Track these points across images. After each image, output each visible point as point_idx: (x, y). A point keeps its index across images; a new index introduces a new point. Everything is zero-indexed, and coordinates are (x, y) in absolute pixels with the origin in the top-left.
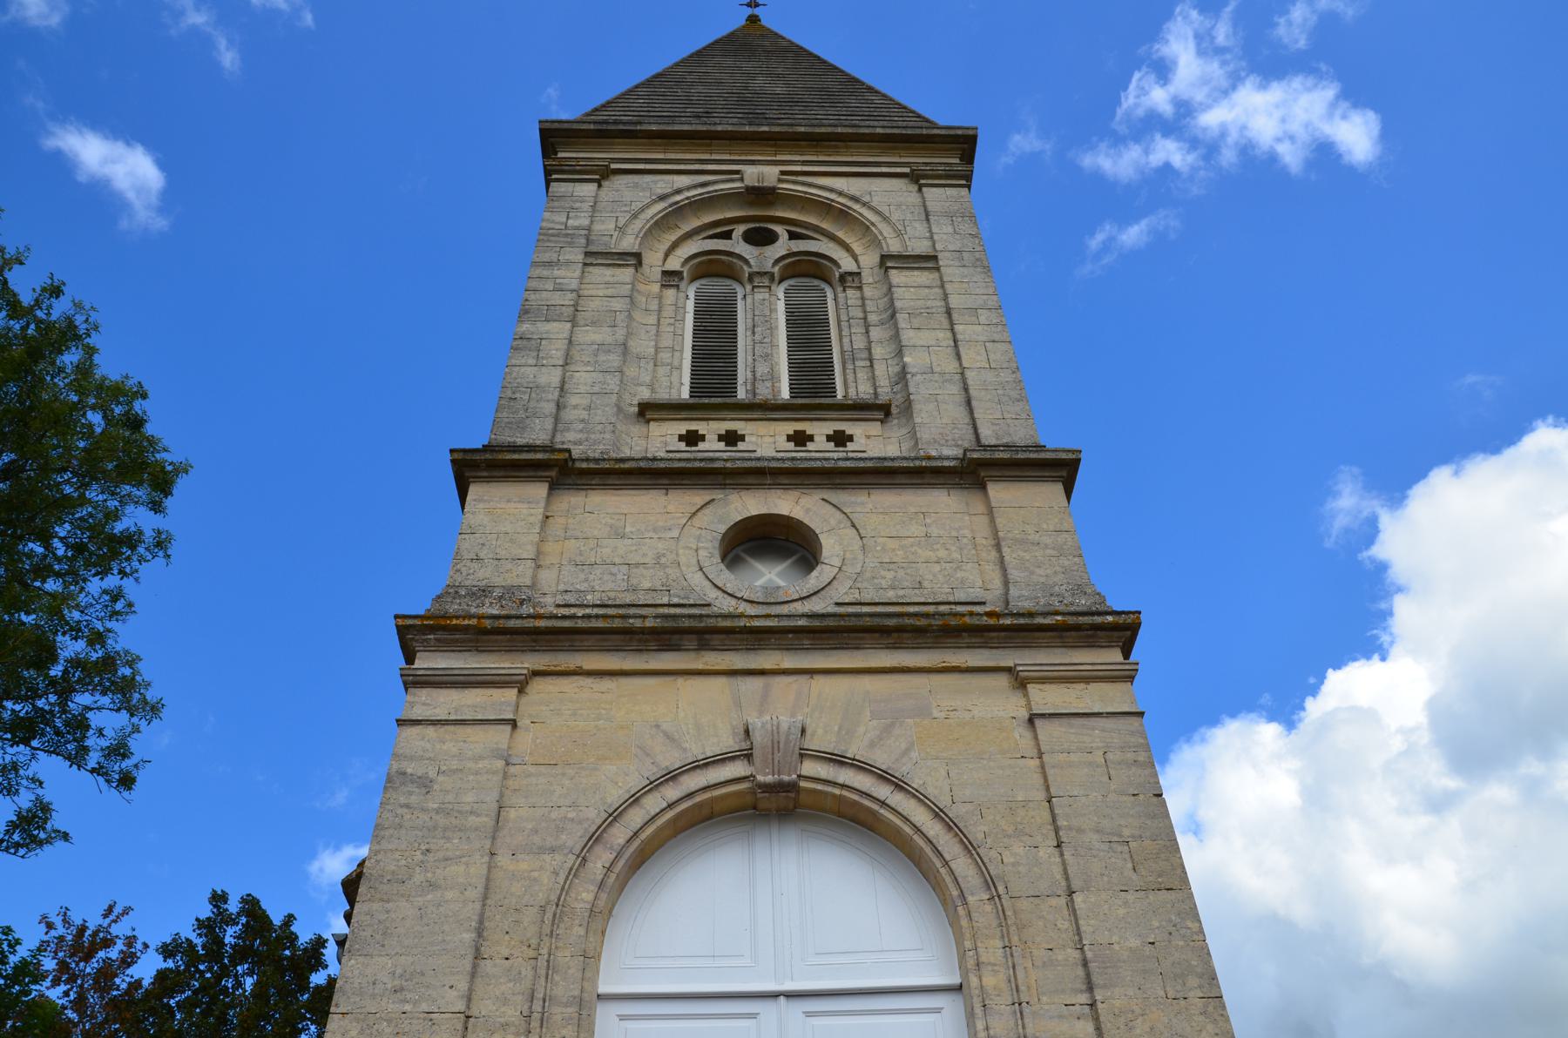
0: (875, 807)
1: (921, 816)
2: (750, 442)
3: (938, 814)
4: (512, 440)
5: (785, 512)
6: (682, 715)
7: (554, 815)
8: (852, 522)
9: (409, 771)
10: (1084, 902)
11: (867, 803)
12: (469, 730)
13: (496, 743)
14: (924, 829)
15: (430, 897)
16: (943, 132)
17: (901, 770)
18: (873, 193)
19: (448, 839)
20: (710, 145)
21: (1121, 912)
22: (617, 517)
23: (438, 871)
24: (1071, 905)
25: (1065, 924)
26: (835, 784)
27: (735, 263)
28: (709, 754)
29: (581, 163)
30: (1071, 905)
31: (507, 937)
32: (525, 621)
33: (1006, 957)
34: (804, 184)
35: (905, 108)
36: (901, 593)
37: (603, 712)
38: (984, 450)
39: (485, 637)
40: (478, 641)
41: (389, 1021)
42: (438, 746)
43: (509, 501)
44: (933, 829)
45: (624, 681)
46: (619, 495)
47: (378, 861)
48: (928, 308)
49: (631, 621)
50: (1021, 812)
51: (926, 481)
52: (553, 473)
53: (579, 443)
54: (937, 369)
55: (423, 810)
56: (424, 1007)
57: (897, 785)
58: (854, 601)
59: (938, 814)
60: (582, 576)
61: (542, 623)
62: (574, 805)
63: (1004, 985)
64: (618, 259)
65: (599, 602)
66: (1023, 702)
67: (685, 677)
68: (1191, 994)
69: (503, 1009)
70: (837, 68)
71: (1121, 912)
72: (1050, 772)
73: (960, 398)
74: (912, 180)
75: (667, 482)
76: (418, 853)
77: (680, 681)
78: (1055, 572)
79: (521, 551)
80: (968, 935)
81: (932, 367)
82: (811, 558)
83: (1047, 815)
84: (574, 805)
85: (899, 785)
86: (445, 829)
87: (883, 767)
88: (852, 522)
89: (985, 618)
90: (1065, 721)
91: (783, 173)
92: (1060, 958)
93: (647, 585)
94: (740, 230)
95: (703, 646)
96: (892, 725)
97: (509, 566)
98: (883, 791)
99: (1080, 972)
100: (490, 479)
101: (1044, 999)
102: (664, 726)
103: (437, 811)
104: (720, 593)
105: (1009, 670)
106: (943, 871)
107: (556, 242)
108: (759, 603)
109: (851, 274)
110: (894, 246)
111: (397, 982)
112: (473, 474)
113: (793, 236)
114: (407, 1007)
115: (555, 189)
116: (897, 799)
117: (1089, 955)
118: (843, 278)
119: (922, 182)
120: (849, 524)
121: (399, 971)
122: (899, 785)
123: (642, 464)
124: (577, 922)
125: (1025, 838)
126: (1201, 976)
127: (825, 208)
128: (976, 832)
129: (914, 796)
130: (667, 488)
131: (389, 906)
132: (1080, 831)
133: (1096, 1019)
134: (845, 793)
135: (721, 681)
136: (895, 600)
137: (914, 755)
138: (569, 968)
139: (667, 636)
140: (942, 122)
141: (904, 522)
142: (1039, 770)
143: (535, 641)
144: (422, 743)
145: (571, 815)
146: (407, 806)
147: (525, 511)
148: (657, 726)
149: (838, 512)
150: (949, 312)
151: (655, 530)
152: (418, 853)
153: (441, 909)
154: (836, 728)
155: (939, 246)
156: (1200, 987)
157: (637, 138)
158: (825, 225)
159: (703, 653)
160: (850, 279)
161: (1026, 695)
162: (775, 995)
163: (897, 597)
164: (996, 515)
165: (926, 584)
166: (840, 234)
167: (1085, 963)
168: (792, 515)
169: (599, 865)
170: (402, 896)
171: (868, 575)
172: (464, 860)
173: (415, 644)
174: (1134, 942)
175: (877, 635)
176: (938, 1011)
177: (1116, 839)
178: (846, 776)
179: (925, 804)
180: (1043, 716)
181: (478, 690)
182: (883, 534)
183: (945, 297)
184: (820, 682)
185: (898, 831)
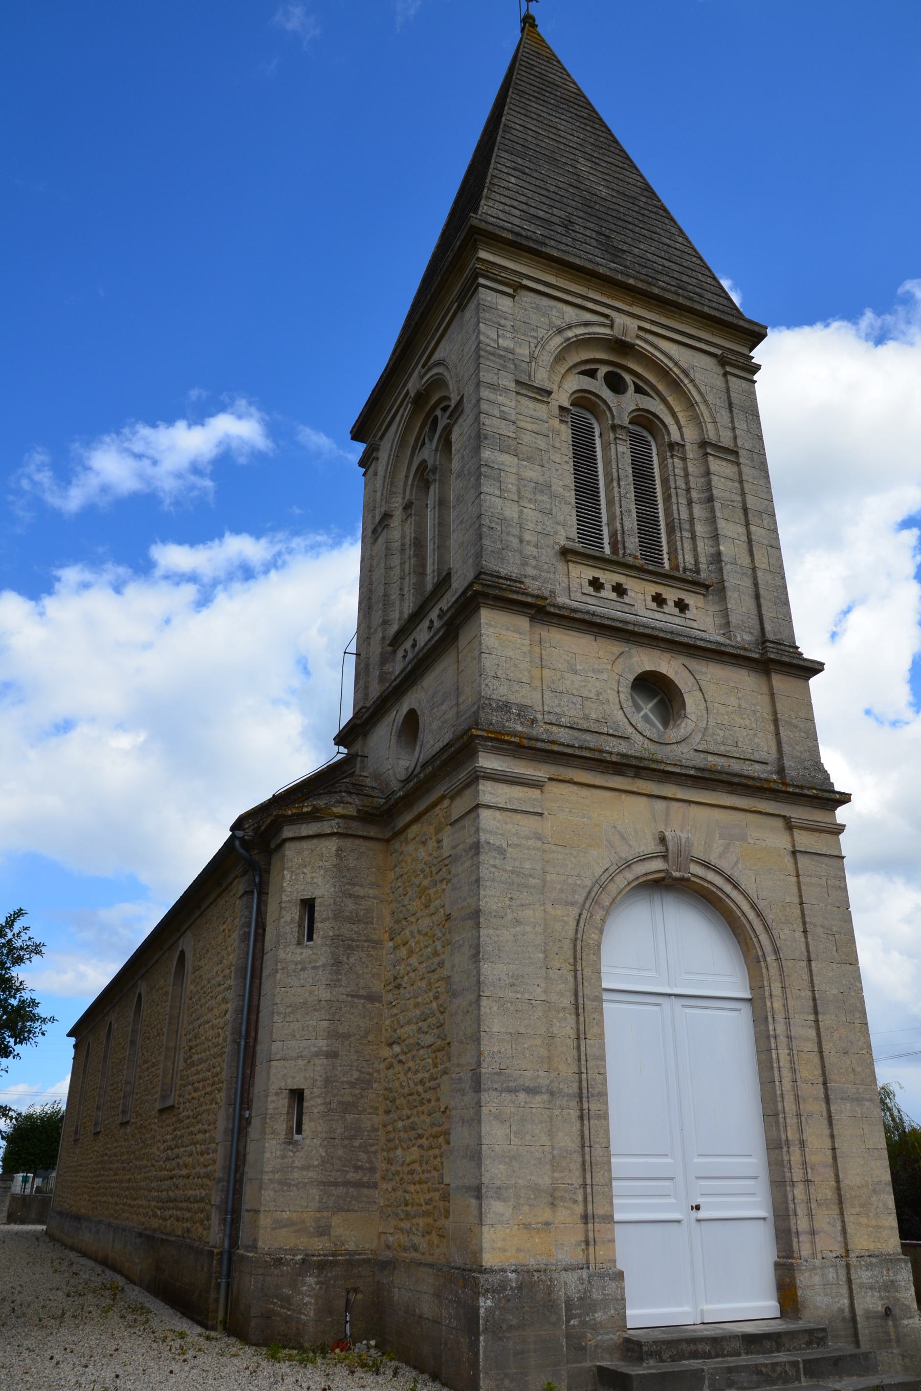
0: (724, 897)
1: (746, 907)
2: (631, 597)
3: (754, 906)
4: (497, 569)
5: (664, 672)
6: (627, 821)
7: (570, 881)
8: (700, 687)
9: (491, 841)
10: (816, 967)
11: (720, 894)
12: (519, 816)
13: (536, 829)
14: (747, 914)
15: (518, 929)
16: (746, 325)
17: (736, 875)
18: (695, 368)
19: (521, 892)
20: (589, 281)
21: (831, 974)
22: (570, 655)
23: (520, 913)
24: (810, 966)
25: (806, 977)
26: (705, 880)
27: (600, 405)
28: (646, 853)
29: (502, 274)
30: (810, 966)
31: (557, 957)
32: (546, 744)
33: (783, 993)
34: (646, 341)
35: (564, 69)
36: (728, 748)
37: (586, 812)
38: (778, 653)
39: (521, 750)
40: (515, 751)
41: (511, 1003)
42: (504, 826)
43: (508, 629)
44: (751, 915)
45: (594, 791)
46: (567, 634)
47: (487, 902)
48: (732, 501)
49: (604, 755)
50: (788, 909)
51: (738, 663)
52: (533, 612)
53: (534, 578)
54: (739, 562)
55: (505, 870)
56: (527, 996)
57: (734, 886)
58: (704, 750)
59: (754, 906)
60: (557, 702)
61: (556, 748)
62: (578, 876)
63: (781, 1008)
64: (537, 393)
65: (569, 725)
66: (789, 839)
67: (627, 794)
68: (856, 1022)
69: (562, 999)
70: (628, 158)
71: (831, 974)
72: (803, 888)
73: (751, 591)
74: (719, 362)
75: (597, 631)
76: (507, 899)
77: (623, 796)
78: (805, 750)
79: (521, 675)
80: (765, 979)
81: (735, 559)
82: (667, 700)
83: (799, 912)
84: (578, 876)
85: (736, 886)
86: (518, 885)
87: (729, 874)
88: (700, 687)
89: (780, 785)
90: (810, 856)
91: (640, 328)
92: (803, 995)
93: (594, 716)
94: (603, 370)
95: (637, 776)
96: (729, 844)
97: (517, 687)
98: (728, 888)
99: (811, 1003)
100: (493, 607)
101: (796, 1016)
102: (619, 828)
103: (512, 872)
104: (633, 729)
105: (784, 817)
106: (755, 940)
107: (494, 362)
108: (655, 741)
109: (678, 444)
110: (711, 436)
111: (511, 980)
112: (484, 601)
113: (638, 390)
114: (519, 996)
115: (483, 296)
116: (734, 894)
117: (817, 996)
118: (672, 446)
119: (728, 369)
120: (698, 688)
121: (510, 974)
122: (736, 886)
123: (587, 617)
124: (592, 952)
125: (790, 925)
126: (860, 1012)
127: (663, 373)
128: (770, 918)
129: (742, 893)
130: (596, 635)
131: (498, 932)
132: (815, 926)
133: (818, 1029)
134: (710, 886)
135: (644, 800)
136: (724, 753)
137: (740, 866)
138: (591, 979)
139: (620, 767)
140: (748, 315)
141: (727, 693)
142: (796, 884)
143: (547, 756)
144: (493, 822)
145: (579, 882)
146: (494, 866)
147: (519, 640)
148: (615, 827)
149: (692, 677)
150: (745, 510)
151: (594, 671)
152: (507, 899)
153: (525, 937)
154: (703, 842)
155: (739, 443)
156: (860, 1018)
157: (540, 257)
158: (660, 387)
159: (636, 779)
160: (677, 448)
161: (792, 835)
162: (670, 995)
163: (729, 751)
164: (777, 700)
165: (740, 744)
166: (670, 399)
167: (814, 999)
168: (668, 675)
169: (598, 918)
170: (504, 926)
171: (710, 731)
172: (531, 907)
173: (478, 746)
174: (835, 992)
175: (726, 785)
176: (739, 1010)
177: (829, 932)
178: (711, 876)
179: (748, 899)
180: (800, 852)
181: (519, 787)
182: (717, 700)
183: (743, 494)
184: (694, 809)
185: (731, 911)
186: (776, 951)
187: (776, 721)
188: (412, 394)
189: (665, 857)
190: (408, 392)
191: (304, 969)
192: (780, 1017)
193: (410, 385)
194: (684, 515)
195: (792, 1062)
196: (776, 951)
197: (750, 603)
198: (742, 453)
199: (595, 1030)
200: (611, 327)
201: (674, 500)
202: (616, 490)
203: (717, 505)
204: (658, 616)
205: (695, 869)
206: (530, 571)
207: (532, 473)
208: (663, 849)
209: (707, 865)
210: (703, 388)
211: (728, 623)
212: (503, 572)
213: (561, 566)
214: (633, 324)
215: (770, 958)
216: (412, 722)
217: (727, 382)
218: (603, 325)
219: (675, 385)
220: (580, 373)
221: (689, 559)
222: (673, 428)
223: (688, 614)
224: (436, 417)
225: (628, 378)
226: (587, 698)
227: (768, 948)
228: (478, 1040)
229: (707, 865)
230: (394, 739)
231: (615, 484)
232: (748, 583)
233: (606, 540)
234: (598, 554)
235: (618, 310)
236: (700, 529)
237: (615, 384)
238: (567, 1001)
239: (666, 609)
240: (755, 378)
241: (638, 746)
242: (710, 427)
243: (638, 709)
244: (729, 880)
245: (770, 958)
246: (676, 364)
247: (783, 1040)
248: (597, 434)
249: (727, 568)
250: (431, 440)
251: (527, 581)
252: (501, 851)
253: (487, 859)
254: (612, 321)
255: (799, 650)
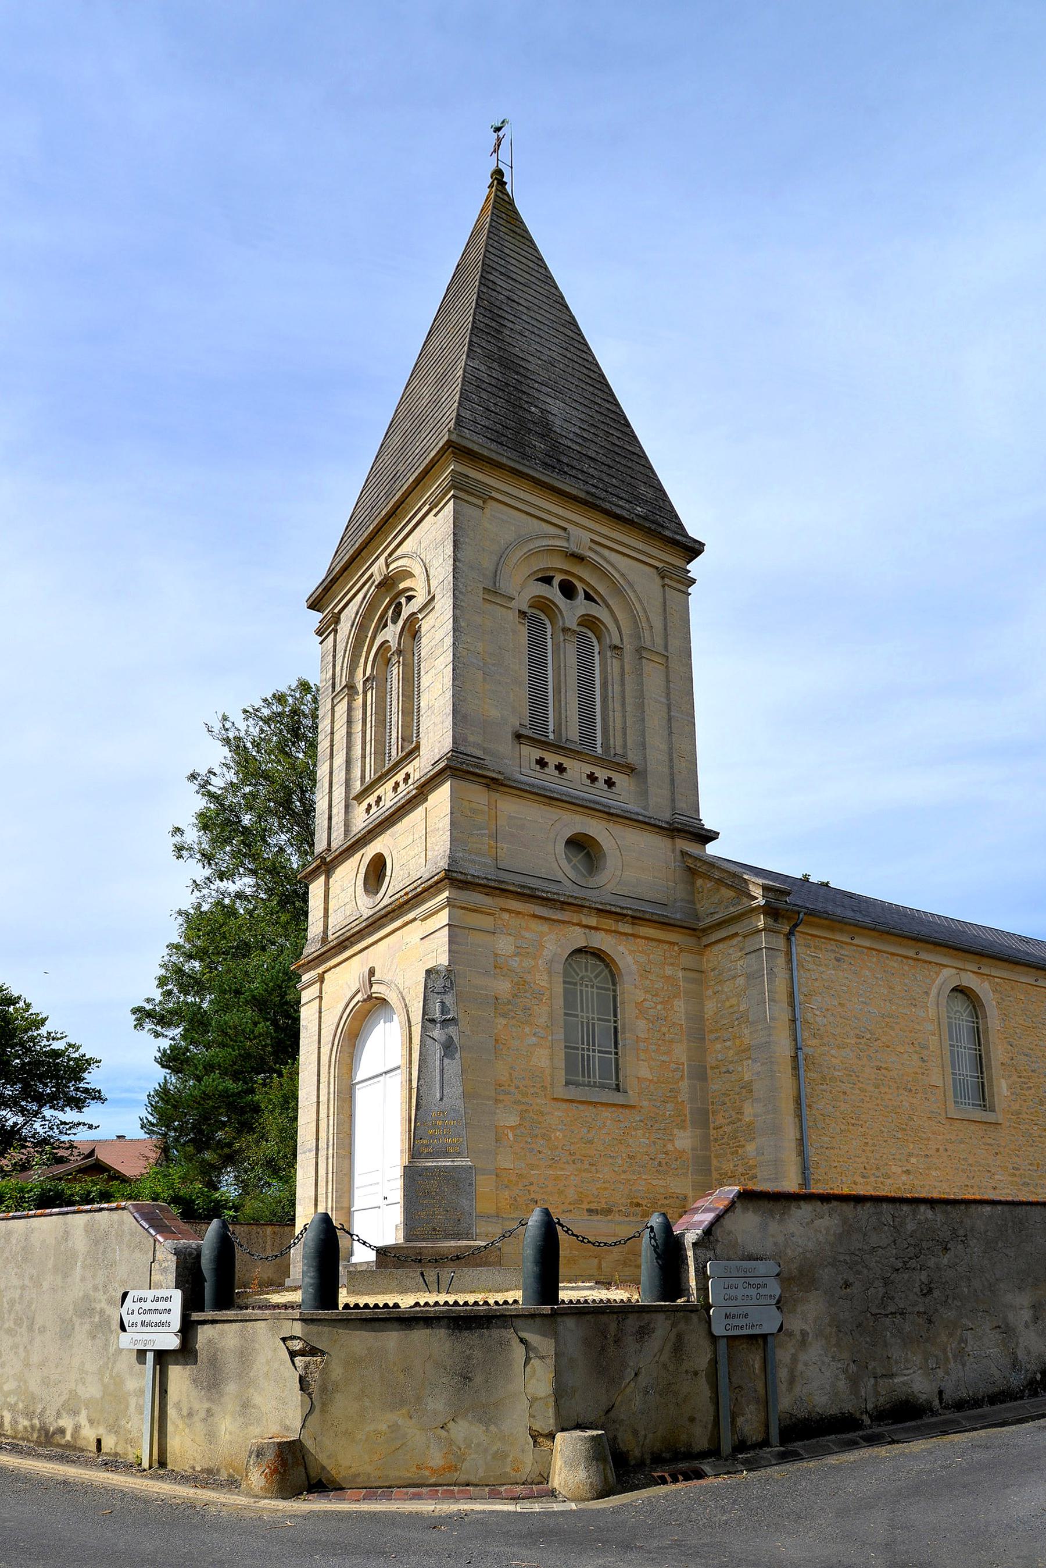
34: (596, 552)
91: (592, 541)
113: (588, 597)
119: (667, 581)
188: (378, 579)
190: (372, 575)
193: (374, 569)
200: (568, 540)
214: (586, 536)
216: (377, 870)
217: (664, 591)
218: (560, 537)
219: (618, 591)
220: (537, 580)
224: (400, 604)
225: (579, 586)
230: (361, 877)
234: (543, 738)
235: (577, 524)
237: (568, 590)
240: (690, 590)
241: (569, 890)
243: (569, 861)
248: (549, 634)
250: (395, 621)
255: (702, 822)
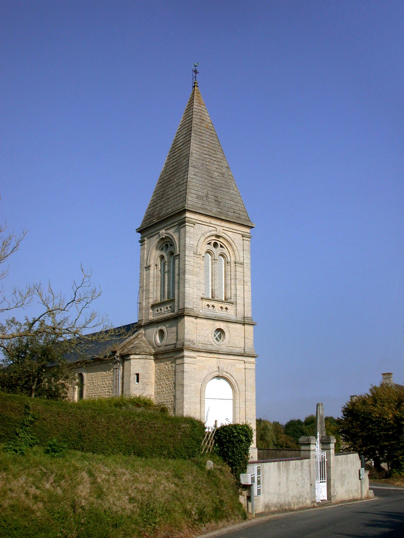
3: (235, 381)
17: (232, 374)
44: (235, 382)
59: (235, 381)
116: (232, 378)
186: (239, 390)
187: (245, 338)
189: (219, 372)
191: (137, 389)
192: (238, 403)
194: (229, 283)
195: (240, 412)
196: (239, 390)
197: (242, 307)
198: (245, 264)
199: (203, 407)
201: (227, 278)
202: (214, 278)
203: (237, 280)
204: (221, 312)
205: (224, 373)
206: (195, 306)
207: (196, 279)
208: (218, 369)
209: (227, 373)
210: (237, 245)
211: (236, 313)
212: (190, 307)
213: (201, 302)
215: (238, 391)
220: (207, 244)
221: (229, 295)
222: (229, 257)
223: (228, 311)
226: (205, 336)
227: (237, 389)
228: (183, 409)
229: (227, 373)
231: (214, 276)
232: (242, 302)
233: (210, 291)
236: (233, 287)
237: (215, 245)
238: (199, 402)
239: (223, 310)
242: (238, 257)
244: (231, 375)
245: (238, 391)
246: (231, 239)
247: (238, 408)
249: (238, 298)
251: (194, 309)
252: (188, 372)
253: (185, 374)
254: (216, 229)
